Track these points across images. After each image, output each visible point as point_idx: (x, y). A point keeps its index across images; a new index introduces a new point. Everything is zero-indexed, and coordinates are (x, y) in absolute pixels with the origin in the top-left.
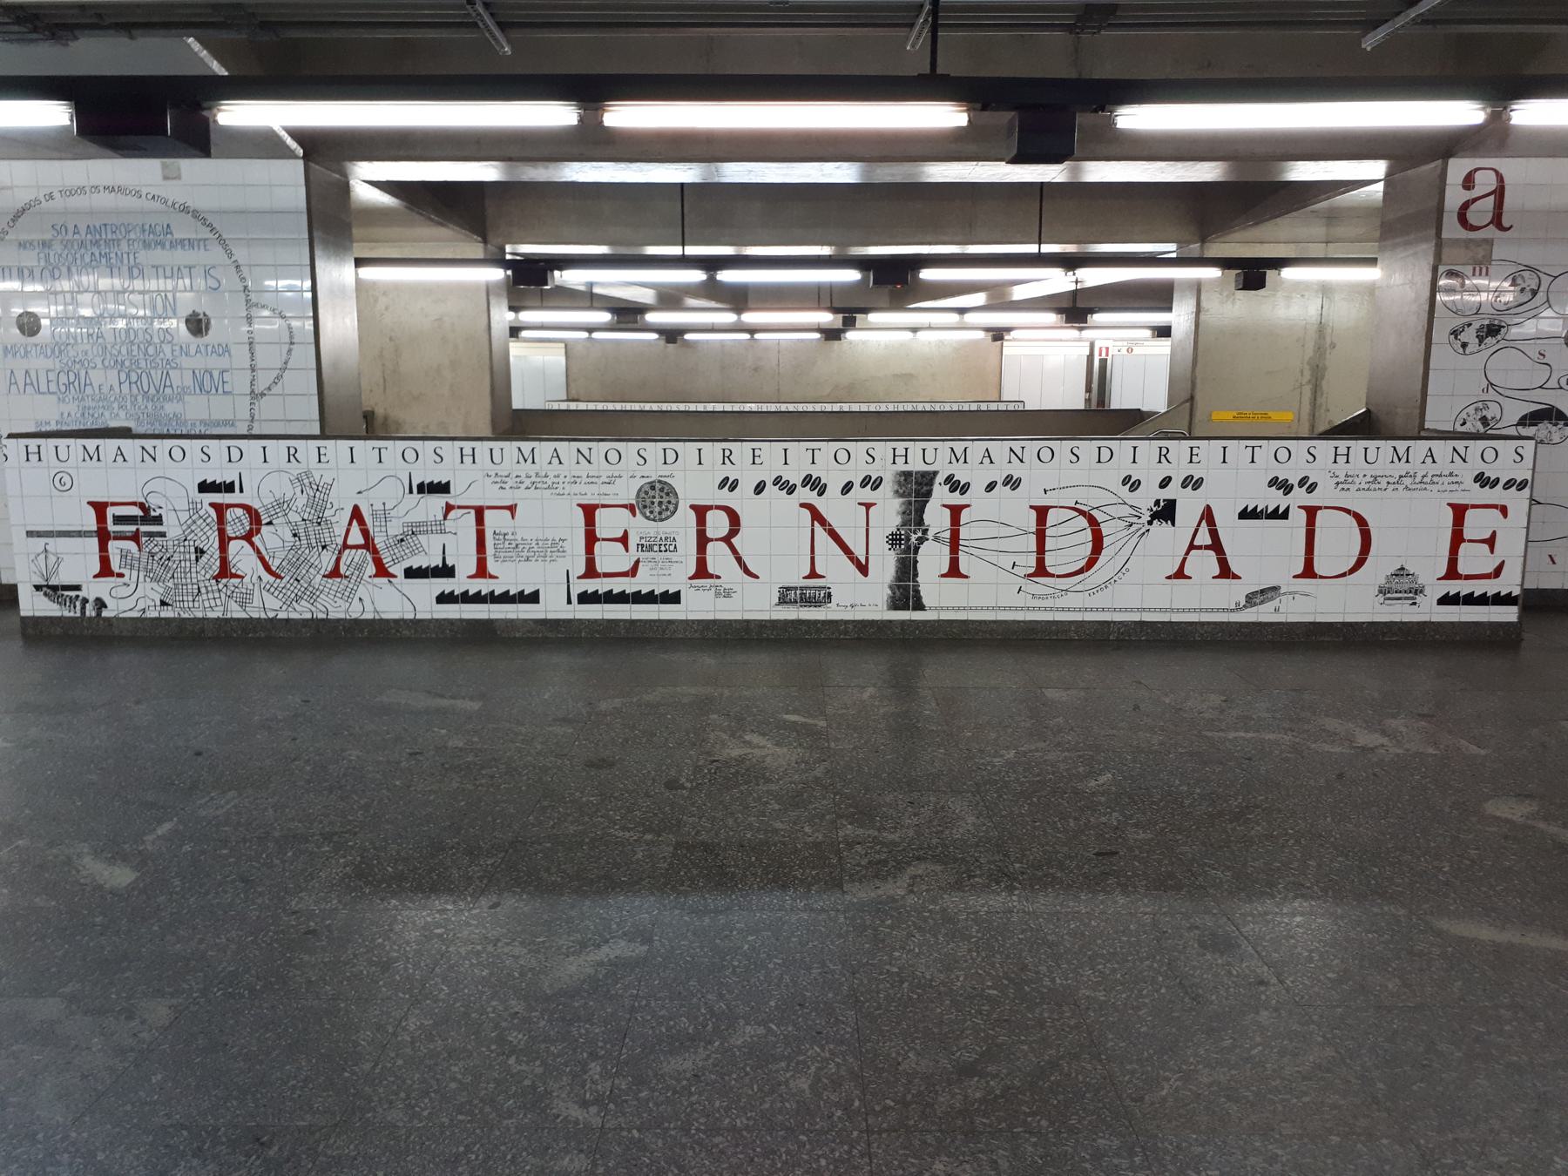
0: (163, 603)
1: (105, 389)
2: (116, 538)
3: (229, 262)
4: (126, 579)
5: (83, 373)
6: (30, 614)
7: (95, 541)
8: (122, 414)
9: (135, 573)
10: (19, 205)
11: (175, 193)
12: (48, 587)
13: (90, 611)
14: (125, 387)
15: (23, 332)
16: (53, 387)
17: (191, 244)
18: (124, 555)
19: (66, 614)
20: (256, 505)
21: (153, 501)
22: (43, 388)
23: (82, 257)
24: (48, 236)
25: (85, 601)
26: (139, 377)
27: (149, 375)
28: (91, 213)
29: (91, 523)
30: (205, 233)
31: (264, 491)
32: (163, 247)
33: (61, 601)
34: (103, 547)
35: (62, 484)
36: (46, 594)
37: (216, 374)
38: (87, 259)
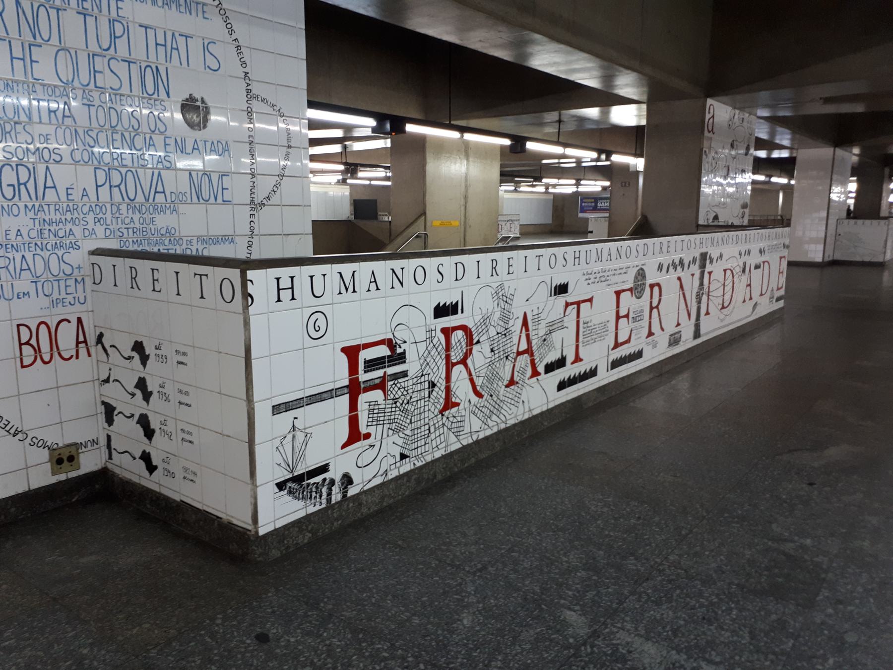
0: (403, 456)
1: (76, 195)
2: (366, 390)
3: (229, 39)
5: (41, 168)
8: (100, 230)
14: (104, 192)
18: (373, 407)
19: (311, 509)
20: (470, 325)
21: (400, 335)
25: (332, 482)
26: (124, 179)
27: (136, 177)
31: (477, 310)
35: (316, 331)
36: (290, 492)
37: (215, 178)
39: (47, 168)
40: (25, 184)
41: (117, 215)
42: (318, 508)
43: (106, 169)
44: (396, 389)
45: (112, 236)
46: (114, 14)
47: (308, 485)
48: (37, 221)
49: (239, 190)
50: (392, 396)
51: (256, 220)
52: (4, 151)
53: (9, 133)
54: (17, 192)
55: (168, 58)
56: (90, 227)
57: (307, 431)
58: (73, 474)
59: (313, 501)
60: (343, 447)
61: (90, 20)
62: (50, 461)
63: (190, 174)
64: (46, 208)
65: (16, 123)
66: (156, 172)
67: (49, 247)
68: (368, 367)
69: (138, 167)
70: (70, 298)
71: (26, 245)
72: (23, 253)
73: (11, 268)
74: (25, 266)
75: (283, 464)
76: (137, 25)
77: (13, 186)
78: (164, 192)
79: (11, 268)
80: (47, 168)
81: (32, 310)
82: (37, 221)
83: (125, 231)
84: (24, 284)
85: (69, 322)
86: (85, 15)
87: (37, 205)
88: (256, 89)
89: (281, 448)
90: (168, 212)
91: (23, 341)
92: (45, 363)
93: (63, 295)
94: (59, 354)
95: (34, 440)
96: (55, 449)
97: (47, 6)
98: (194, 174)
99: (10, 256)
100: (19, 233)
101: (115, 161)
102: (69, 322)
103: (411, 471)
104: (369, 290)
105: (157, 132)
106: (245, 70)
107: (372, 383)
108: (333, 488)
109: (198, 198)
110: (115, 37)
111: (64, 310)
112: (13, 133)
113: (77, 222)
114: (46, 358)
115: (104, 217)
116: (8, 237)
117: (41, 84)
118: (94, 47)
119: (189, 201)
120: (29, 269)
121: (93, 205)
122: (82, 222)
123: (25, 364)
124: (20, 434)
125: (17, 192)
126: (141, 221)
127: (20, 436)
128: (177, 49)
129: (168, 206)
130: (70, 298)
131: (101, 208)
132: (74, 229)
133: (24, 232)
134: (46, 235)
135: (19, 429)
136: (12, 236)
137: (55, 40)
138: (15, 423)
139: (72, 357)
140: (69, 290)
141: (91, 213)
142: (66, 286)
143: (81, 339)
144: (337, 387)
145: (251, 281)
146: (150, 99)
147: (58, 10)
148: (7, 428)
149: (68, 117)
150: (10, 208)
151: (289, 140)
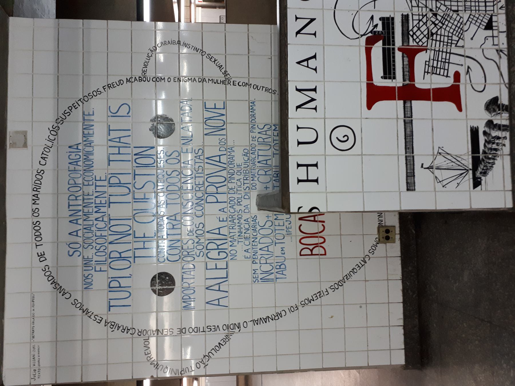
0: (489, 26)
1: (224, 216)
2: (412, 78)
3: (104, 94)
4: (462, 71)
5: (208, 236)
6: (509, 195)
7: (416, 104)
8: (244, 202)
9: (454, 59)
10: (49, 287)
11: (39, 138)
12: (475, 169)
13: (503, 119)
15: (168, 292)
16: (222, 264)
17: (87, 127)
18: (431, 69)
19: (507, 149)
21: (364, 27)
22: (223, 274)
23: (99, 229)
24: (79, 261)
25: (490, 124)
26: (212, 184)
27: (210, 175)
28: (57, 218)
29: (392, 108)
30: (77, 114)
32: (91, 153)
33: (492, 155)
34: (424, 95)
35: (346, 140)
36: (485, 173)
37: (207, 115)
38: (101, 225)
39: (207, 232)
40: (218, 246)
41: (235, 190)
42: (507, 142)
43: (206, 195)
44: (418, 33)
45: (249, 194)
46: (105, 183)
47: (484, 152)
48: (240, 240)
49: (215, 93)
50: (425, 40)
51: (238, 80)
52: (199, 256)
53: (188, 253)
54: (223, 251)
55: (127, 146)
56: (243, 208)
57: (436, 153)
58: (398, 230)
59: (500, 147)
60: (460, 109)
61: (112, 199)
62: (385, 243)
63: (206, 135)
64: (231, 234)
65: (182, 249)
66: (206, 161)
67: (255, 234)
68: (390, 73)
69: (204, 173)
70: (286, 224)
71: (254, 247)
72: (258, 249)
73: (266, 257)
74: (266, 249)
75: (458, 181)
76: (109, 312)
77: (219, 252)
78: (220, 156)
79: (266, 257)
80: (207, 232)
81: (292, 246)
82: (240, 240)
83: (246, 185)
84: (276, 250)
85: (301, 225)
86: (110, 203)
87: (230, 239)
88: (138, 73)
89: (445, 183)
90: (233, 154)
91: (310, 253)
92: (324, 242)
93: (284, 228)
94: (321, 243)
95: (370, 251)
96: (379, 240)
97: (109, 226)
98: (206, 132)
99: (259, 257)
100: (246, 251)
101: (201, 189)
102: (301, 225)
103: (507, 14)
104: (315, 70)
105: (179, 158)
106: (125, 81)
107: (407, 69)
108: (495, 122)
109: (223, 129)
110: (120, 183)
111: (293, 227)
112: (189, 251)
113: (240, 216)
114: (322, 240)
115: (237, 199)
116: (249, 257)
117: (158, 233)
118: (129, 198)
119: (225, 137)
120: (267, 246)
121: (229, 205)
122: (240, 213)
123: (324, 253)
124: (365, 259)
125: (223, 251)
126: (239, 173)
127: (367, 259)
128: (120, 138)
129: (229, 154)
130: (286, 224)
131: (231, 200)
132: (244, 218)
133: (246, 248)
134: (248, 235)
135: (363, 259)
136: (248, 255)
137: (130, 223)
138: (358, 261)
139: (323, 225)
140: (281, 224)
141: (234, 207)
142: (279, 225)
143: (312, 218)
144: (403, 116)
145: (299, 208)
146: (157, 161)
147: (110, 220)
148: (361, 266)
149: (175, 218)
150: (232, 255)
151: (173, 43)
